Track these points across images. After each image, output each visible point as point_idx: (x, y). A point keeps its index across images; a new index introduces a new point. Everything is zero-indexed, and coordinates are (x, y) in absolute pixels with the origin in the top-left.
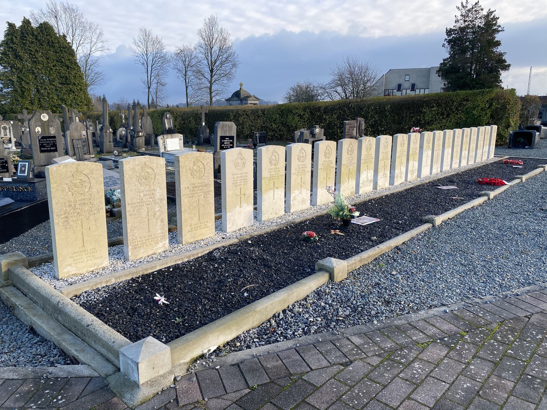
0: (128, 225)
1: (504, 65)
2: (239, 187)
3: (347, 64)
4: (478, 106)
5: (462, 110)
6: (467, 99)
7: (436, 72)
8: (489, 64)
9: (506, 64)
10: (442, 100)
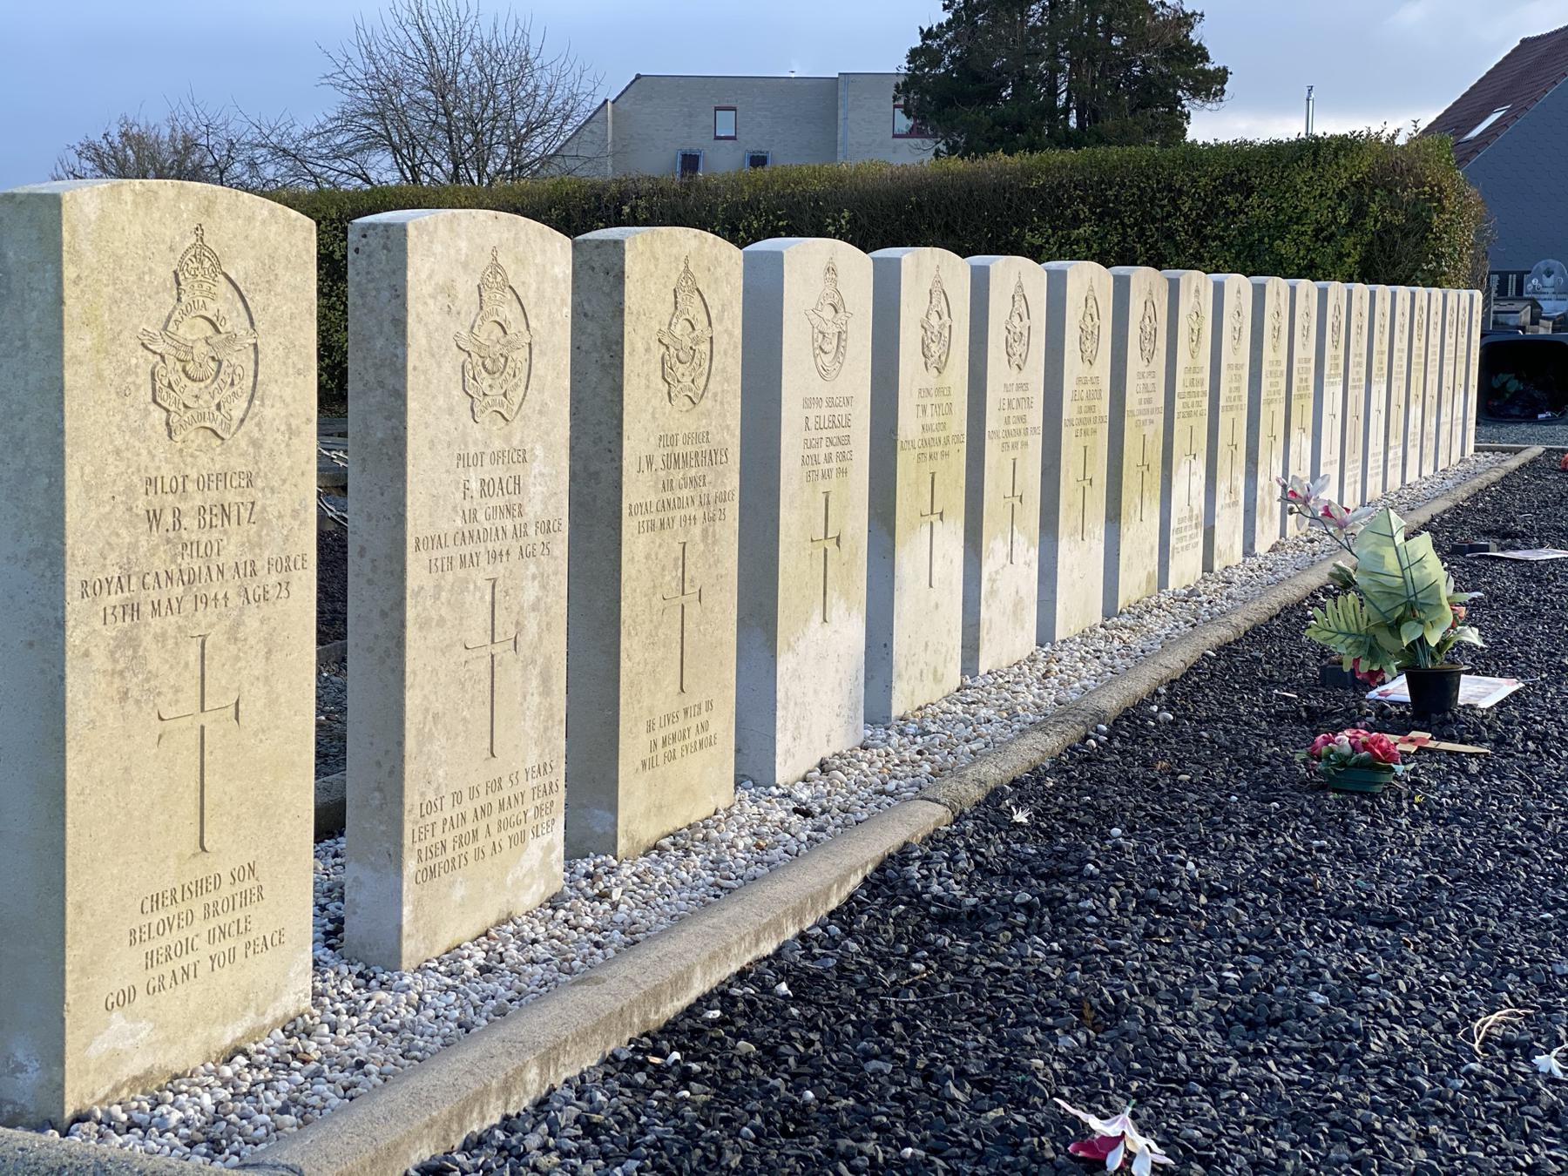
0: (408, 694)
1: (1203, 72)
2: (480, 576)
3: (414, 32)
4: (1299, 219)
5: (1221, 239)
6: (1242, 182)
7: (893, 92)
8: (1133, 63)
9: (1210, 67)
10: (1122, 185)
